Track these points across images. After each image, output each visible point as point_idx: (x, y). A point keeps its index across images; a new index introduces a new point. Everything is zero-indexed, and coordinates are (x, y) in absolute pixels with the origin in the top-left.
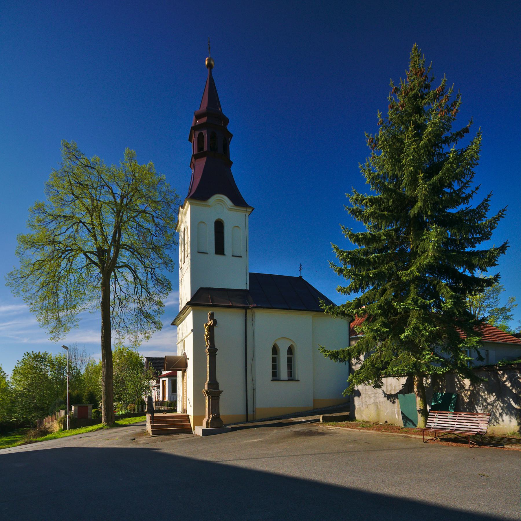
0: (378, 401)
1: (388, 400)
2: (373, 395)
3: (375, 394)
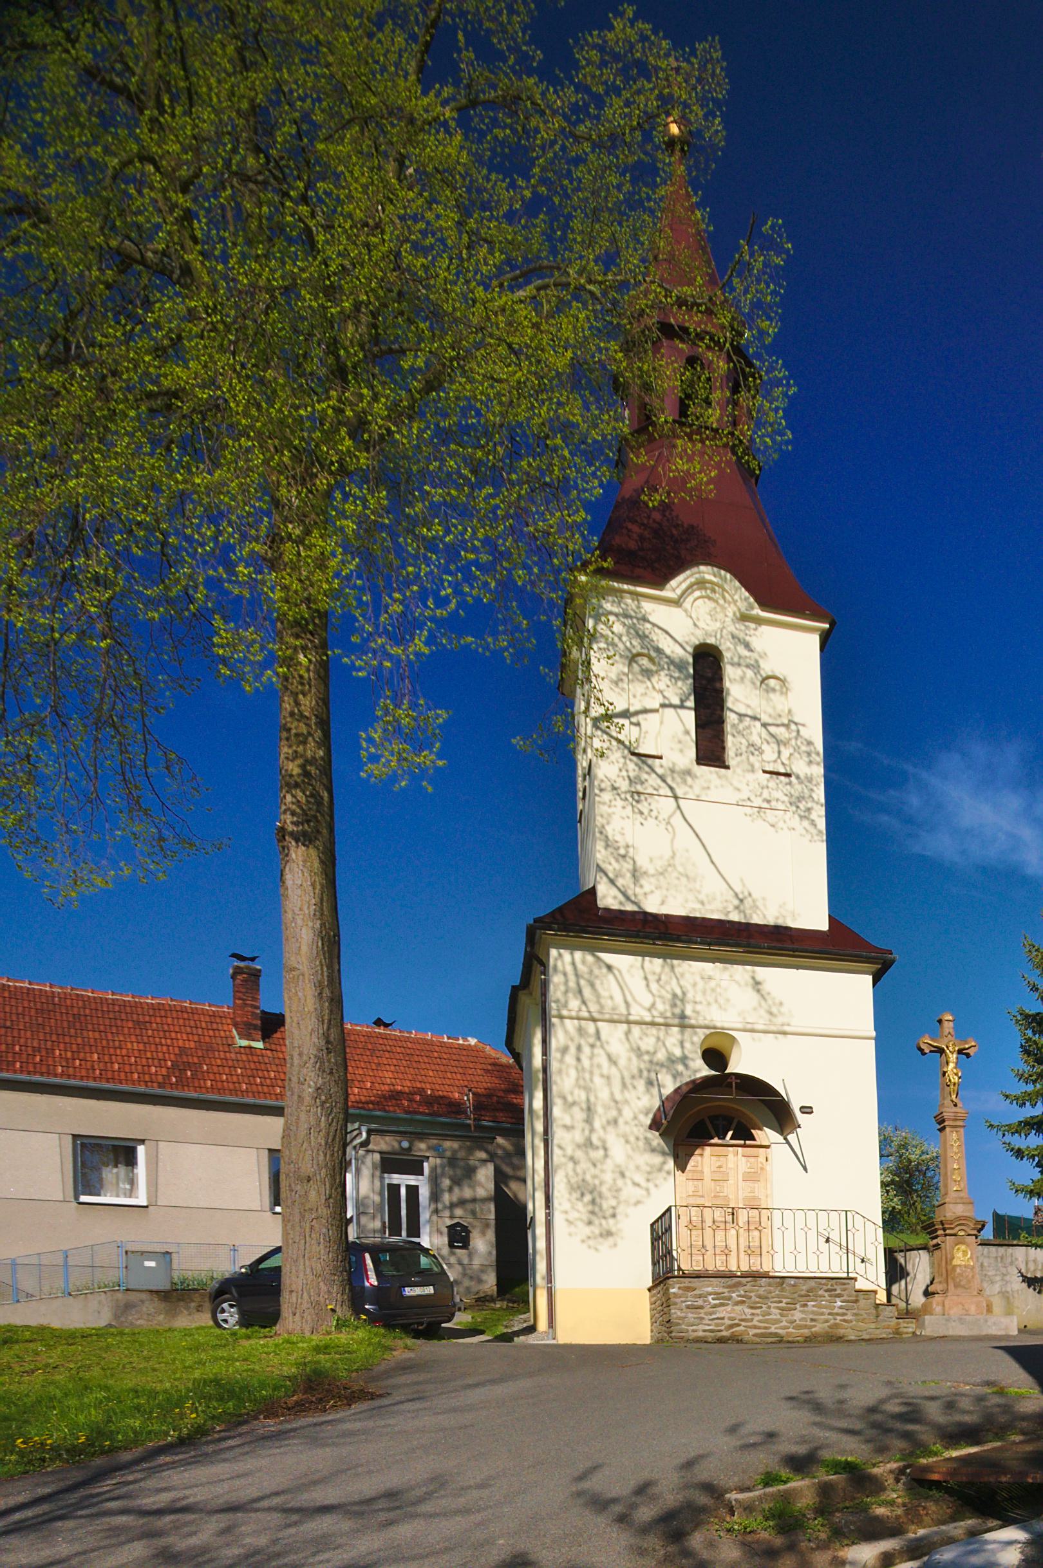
0: (1009, 1289)
1: (1029, 1287)
2: (998, 1278)
3: (1004, 1275)
